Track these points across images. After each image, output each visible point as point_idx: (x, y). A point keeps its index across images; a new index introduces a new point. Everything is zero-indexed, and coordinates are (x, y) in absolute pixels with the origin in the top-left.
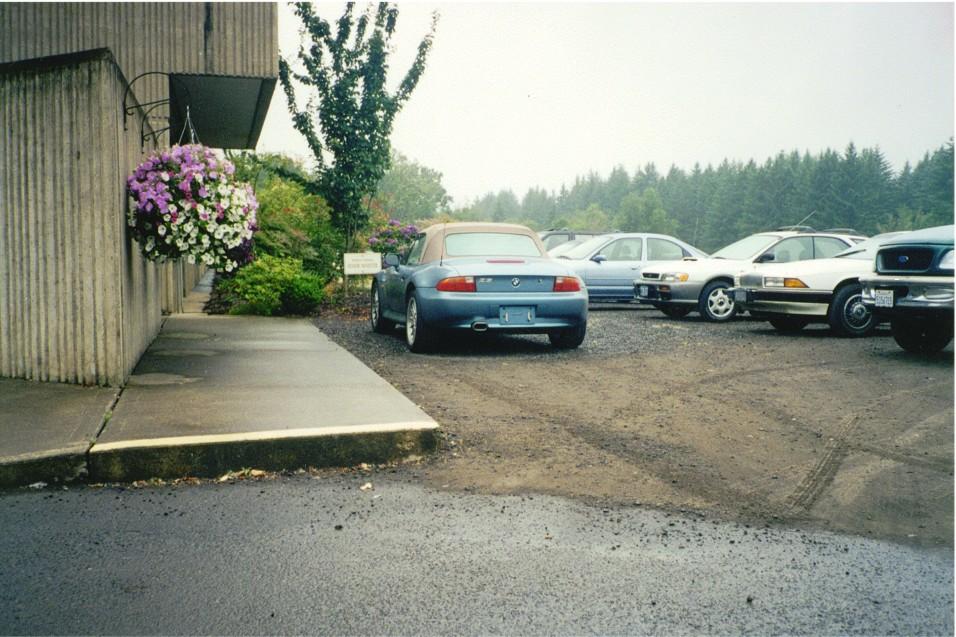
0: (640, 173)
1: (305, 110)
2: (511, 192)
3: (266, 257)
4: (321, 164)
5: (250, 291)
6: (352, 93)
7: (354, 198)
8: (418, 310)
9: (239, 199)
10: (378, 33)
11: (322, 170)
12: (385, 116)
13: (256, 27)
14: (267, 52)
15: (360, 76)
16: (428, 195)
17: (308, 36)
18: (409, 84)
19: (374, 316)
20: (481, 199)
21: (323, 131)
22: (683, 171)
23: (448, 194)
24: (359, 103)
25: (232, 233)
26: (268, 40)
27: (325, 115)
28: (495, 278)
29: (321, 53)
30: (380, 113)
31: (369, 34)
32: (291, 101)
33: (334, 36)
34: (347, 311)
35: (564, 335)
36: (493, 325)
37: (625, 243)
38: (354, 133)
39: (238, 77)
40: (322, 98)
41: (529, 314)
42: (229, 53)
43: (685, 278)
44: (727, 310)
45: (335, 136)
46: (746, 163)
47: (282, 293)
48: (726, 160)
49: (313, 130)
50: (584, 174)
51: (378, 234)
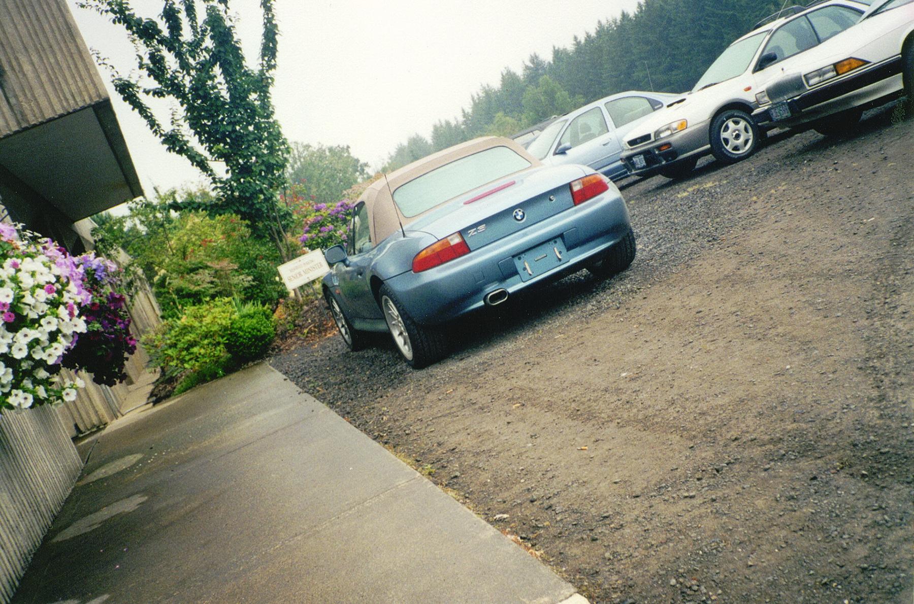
0: (527, 68)
1: (172, 128)
2: (418, 136)
3: (190, 309)
4: (214, 179)
5: (187, 358)
6: (214, 87)
7: (267, 200)
8: (398, 310)
9: (33, 274)
10: (212, 9)
11: (219, 185)
12: (260, 96)
13: (56, 48)
14: (82, 73)
15: (214, 65)
16: (341, 168)
17: (140, 43)
18: (269, 49)
19: (343, 330)
20: (393, 153)
21: (202, 142)
22: (565, 49)
23: (362, 161)
24: (225, 95)
25: (44, 338)
26: (76, 57)
27: (195, 123)
28: (487, 221)
29: (162, 58)
30: (253, 96)
31: (201, 15)
32: (152, 123)
33: (166, 33)
34: (310, 332)
35: (605, 263)
36: (514, 286)
37: (581, 121)
38: (234, 131)
39: (61, 116)
40: (185, 106)
41: (557, 249)
42: (38, 92)
43: (684, 124)
44: (746, 142)
45: (218, 141)
46: (619, 17)
47: (225, 344)
48: (599, 22)
49: (189, 145)
50: (477, 91)
51: (307, 228)
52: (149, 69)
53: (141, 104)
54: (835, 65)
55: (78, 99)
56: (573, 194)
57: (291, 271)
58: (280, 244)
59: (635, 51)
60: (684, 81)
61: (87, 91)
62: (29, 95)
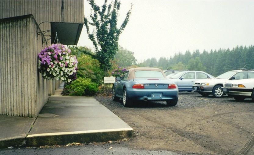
0: (194, 52)
2: (155, 58)
3: (80, 78)
5: (75, 88)
6: (106, 28)
10: (114, 10)
11: (97, 52)
12: (117, 35)
16: (130, 59)
17: (93, 11)
18: (124, 25)
19: (113, 96)
21: (98, 40)
22: (207, 52)
23: (136, 59)
24: (109, 31)
25: (70, 71)
28: (150, 84)
29: (97, 16)
30: (115, 34)
31: (112, 10)
32: (88, 30)
33: (101, 11)
34: (105, 94)
35: (171, 102)
36: (149, 99)
37: (190, 74)
38: (107, 40)
40: (97, 30)
41: (160, 95)
42: (69, 16)
43: (208, 84)
44: (221, 94)
45: (101, 41)
46: (226, 49)
48: (220, 49)
50: (177, 53)
52: (92, 18)
53: (87, 25)
54: (239, 85)
55: (77, 21)
56: (168, 86)
57: (107, 79)
58: (106, 72)
59: (227, 61)
60: (216, 75)
61: (80, 20)
62: (67, 15)
